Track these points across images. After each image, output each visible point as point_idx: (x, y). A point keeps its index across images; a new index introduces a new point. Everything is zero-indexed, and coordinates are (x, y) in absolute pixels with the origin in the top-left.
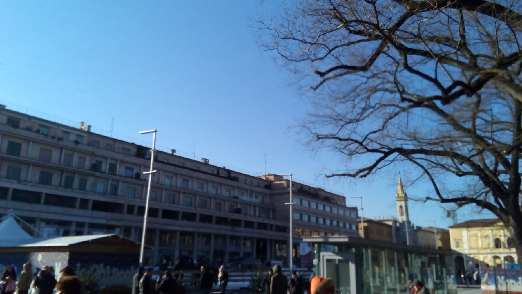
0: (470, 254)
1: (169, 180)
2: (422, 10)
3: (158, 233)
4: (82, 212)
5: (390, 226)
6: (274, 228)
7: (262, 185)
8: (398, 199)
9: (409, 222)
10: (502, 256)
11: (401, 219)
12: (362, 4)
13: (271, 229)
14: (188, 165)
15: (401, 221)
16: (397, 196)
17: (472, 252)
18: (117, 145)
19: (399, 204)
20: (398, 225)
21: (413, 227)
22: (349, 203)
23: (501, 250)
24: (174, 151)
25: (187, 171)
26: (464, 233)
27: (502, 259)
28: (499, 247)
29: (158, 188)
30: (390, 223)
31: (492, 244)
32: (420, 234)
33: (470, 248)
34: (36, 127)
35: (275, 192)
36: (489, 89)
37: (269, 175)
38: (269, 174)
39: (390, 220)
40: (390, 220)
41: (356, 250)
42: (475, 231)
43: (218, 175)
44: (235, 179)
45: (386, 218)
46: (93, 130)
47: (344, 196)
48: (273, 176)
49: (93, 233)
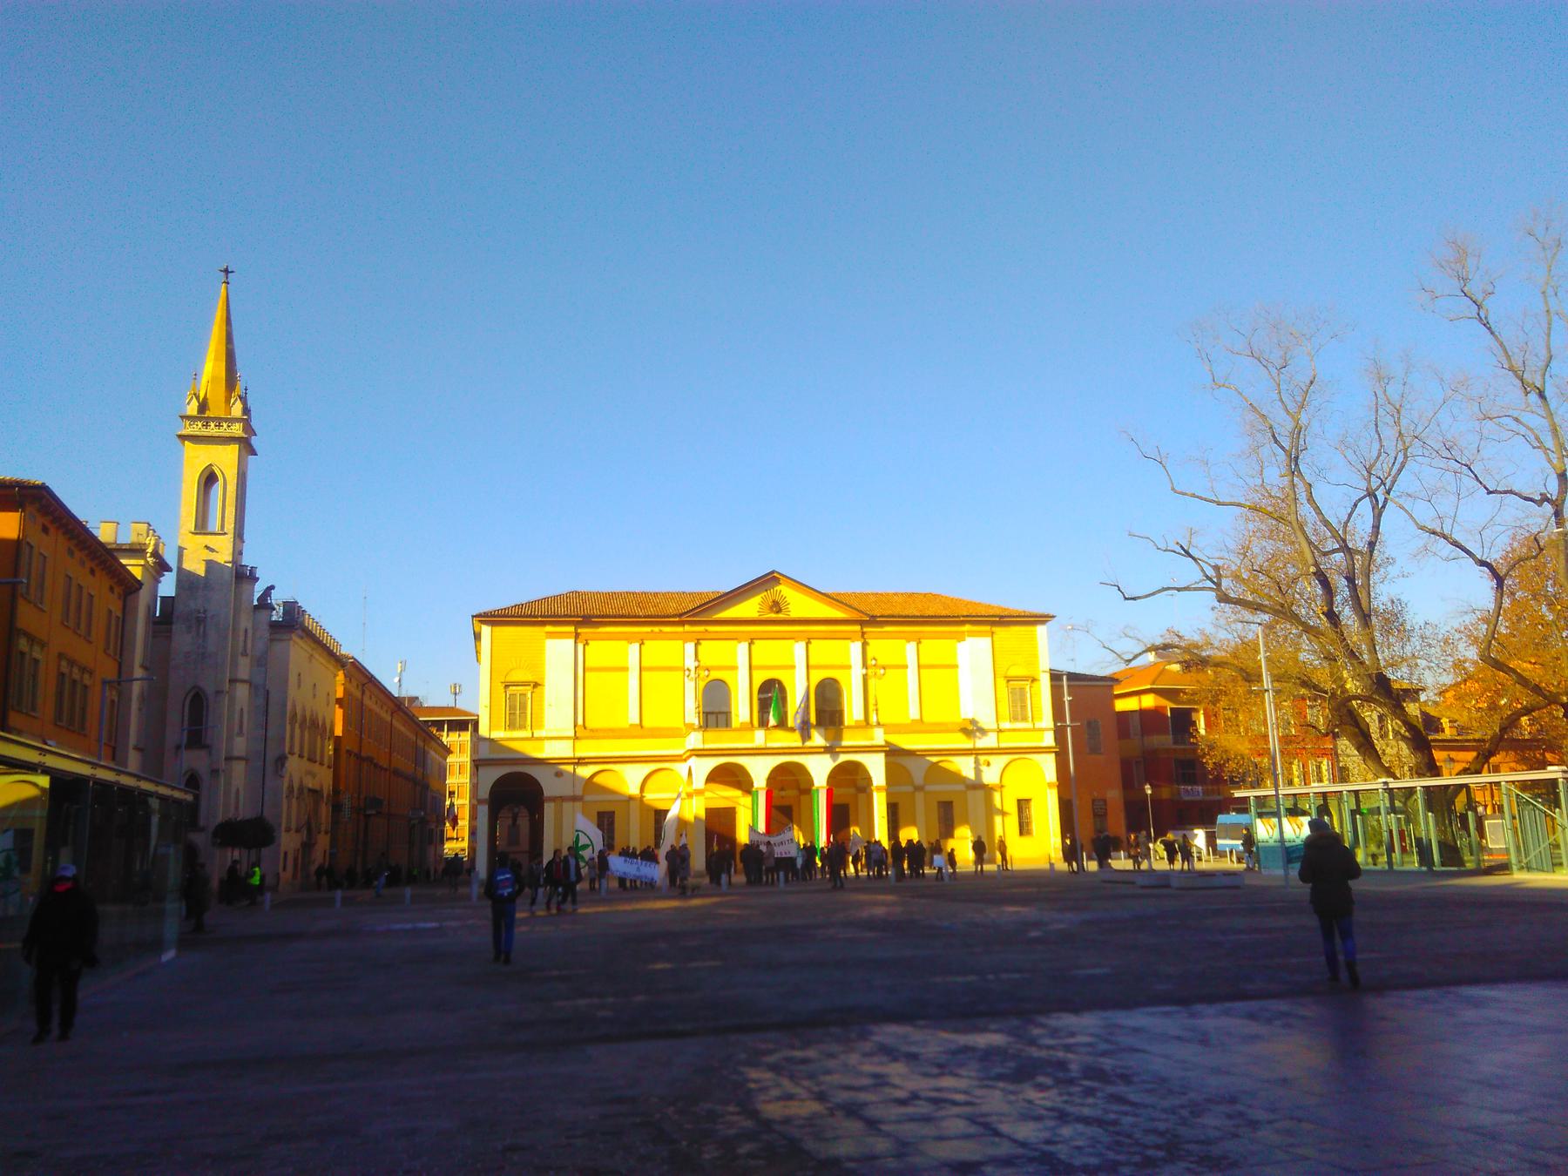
0: (581, 761)
9: (244, 576)
15: (195, 565)
16: (192, 409)
17: (587, 749)
19: (197, 458)
21: (264, 604)
32: (297, 650)
33: (581, 731)
42: (609, 648)
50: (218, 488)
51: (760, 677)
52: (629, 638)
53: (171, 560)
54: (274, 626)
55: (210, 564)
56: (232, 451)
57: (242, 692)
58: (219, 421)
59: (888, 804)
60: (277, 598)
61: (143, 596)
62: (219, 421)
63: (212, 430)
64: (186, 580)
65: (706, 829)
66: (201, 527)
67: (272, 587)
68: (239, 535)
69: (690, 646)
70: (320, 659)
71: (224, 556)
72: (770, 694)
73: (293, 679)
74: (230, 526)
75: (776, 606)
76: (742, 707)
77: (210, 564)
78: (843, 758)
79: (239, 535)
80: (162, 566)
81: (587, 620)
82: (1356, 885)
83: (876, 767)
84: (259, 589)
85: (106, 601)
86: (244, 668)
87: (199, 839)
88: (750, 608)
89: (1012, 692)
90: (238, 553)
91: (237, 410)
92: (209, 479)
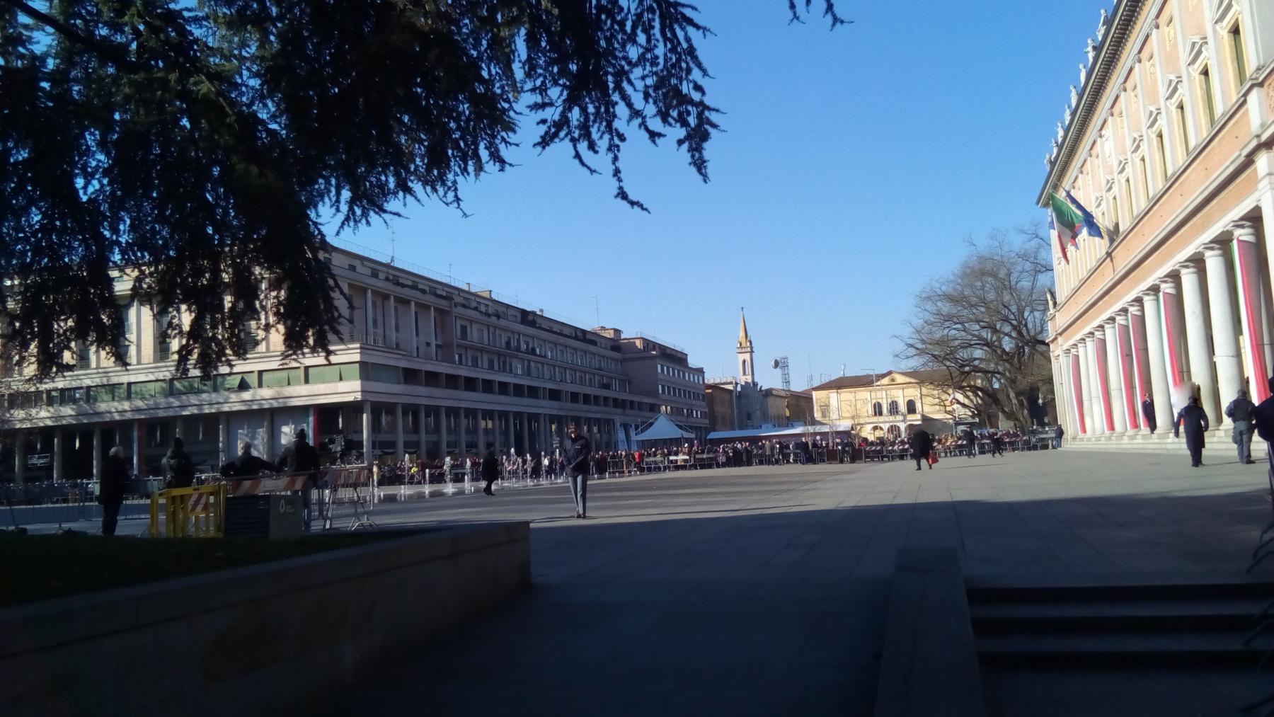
1: (130, 292)
4: (502, 398)
6: (611, 402)
7: (610, 344)
8: (740, 350)
9: (755, 384)
10: (886, 427)
11: (743, 380)
12: (1002, 336)
13: (597, 403)
16: (739, 345)
19: (741, 357)
20: (739, 389)
22: (693, 362)
23: (881, 419)
24: (542, 311)
25: (555, 335)
26: (833, 397)
29: (573, 370)
30: (730, 387)
31: (871, 411)
32: (770, 401)
34: (474, 305)
35: (627, 356)
38: (602, 327)
40: (731, 383)
42: (847, 395)
43: (576, 338)
44: (593, 343)
45: (724, 380)
46: (495, 297)
48: (612, 332)
49: (794, 424)
50: (746, 363)
51: (907, 399)
53: (738, 382)
54: (763, 395)
55: (746, 382)
57: (758, 412)
58: (745, 348)
60: (763, 389)
61: (734, 394)
62: (745, 348)
63: (744, 350)
64: (742, 386)
65: (476, 378)
66: (744, 373)
68: (753, 374)
69: (884, 392)
72: (894, 409)
74: (750, 373)
75: (893, 380)
76: (903, 407)
78: (909, 423)
79: (753, 374)
80: (737, 384)
85: (727, 396)
87: (244, 67)
88: (886, 381)
89: (822, 410)
91: (748, 344)
92: (744, 362)
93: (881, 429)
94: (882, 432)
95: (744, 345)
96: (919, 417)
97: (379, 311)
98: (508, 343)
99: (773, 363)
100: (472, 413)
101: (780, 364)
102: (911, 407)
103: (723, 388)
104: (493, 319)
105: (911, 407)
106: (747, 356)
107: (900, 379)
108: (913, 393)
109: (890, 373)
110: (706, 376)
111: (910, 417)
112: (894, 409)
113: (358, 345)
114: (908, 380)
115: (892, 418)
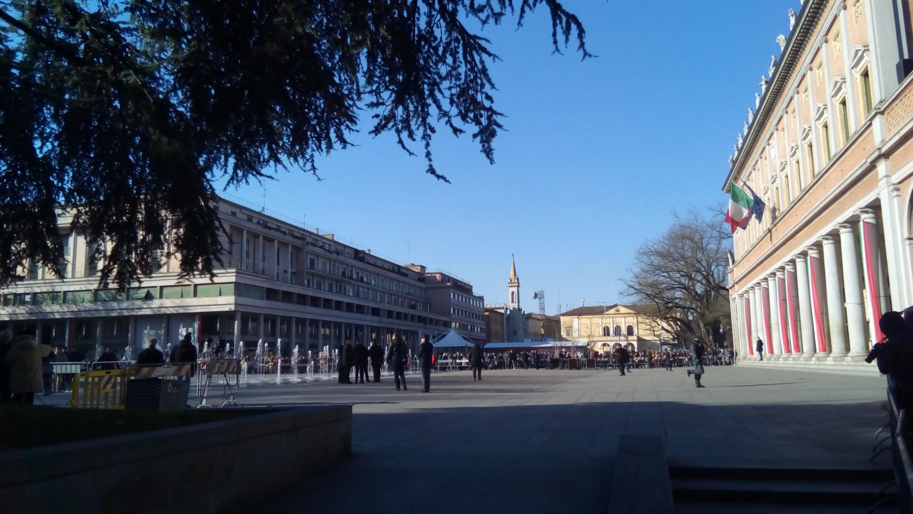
2: (730, 261)
3: (366, 327)
4: (338, 313)
5: (502, 314)
8: (510, 285)
9: (520, 310)
10: (612, 344)
11: (512, 306)
14: (386, 266)
16: (509, 281)
18: (347, 250)
20: (508, 312)
22: (476, 292)
23: (609, 338)
24: (369, 250)
26: (575, 321)
27: (611, 346)
28: (239, 298)
30: (502, 311)
31: (601, 333)
32: (530, 322)
34: (320, 244)
36: (564, 37)
37: (413, 265)
39: (503, 308)
40: (503, 308)
41: (376, 335)
42: (585, 320)
43: (393, 271)
45: (498, 306)
46: (336, 239)
47: (471, 284)
48: (419, 268)
51: (627, 325)
52: (588, 318)
55: (514, 308)
56: (516, 288)
57: (521, 330)
59: (297, 304)
60: (526, 313)
63: (513, 285)
66: (513, 302)
67: (582, 61)
68: (519, 302)
69: (611, 319)
70: (536, 321)
71: (516, 307)
72: (618, 331)
73: (530, 327)
75: (618, 311)
77: (514, 308)
79: (519, 302)
80: (507, 309)
81: (580, 315)
82: (61, 259)
83: (635, 344)
84: (522, 312)
85: (500, 318)
86: (521, 326)
88: (612, 311)
89: (567, 330)
90: (519, 305)
92: (513, 293)
93: (609, 345)
94: (609, 348)
95: (513, 281)
96: (635, 338)
97: (251, 246)
98: (344, 273)
99: (533, 295)
100: (314, 323)
101: (538, 296)
102: (630, 331)
103: (497, 312)
104: (334, 255)
105: (630, 331)
106: (515, 289)
107: (623, 310)
108: (632, 321)
109: (616, 306)
110: (485, 302)
111: (630, 338)
112: (618, 331)
113: (234, 270)
114: (628, 311)
115: (617, 338)
